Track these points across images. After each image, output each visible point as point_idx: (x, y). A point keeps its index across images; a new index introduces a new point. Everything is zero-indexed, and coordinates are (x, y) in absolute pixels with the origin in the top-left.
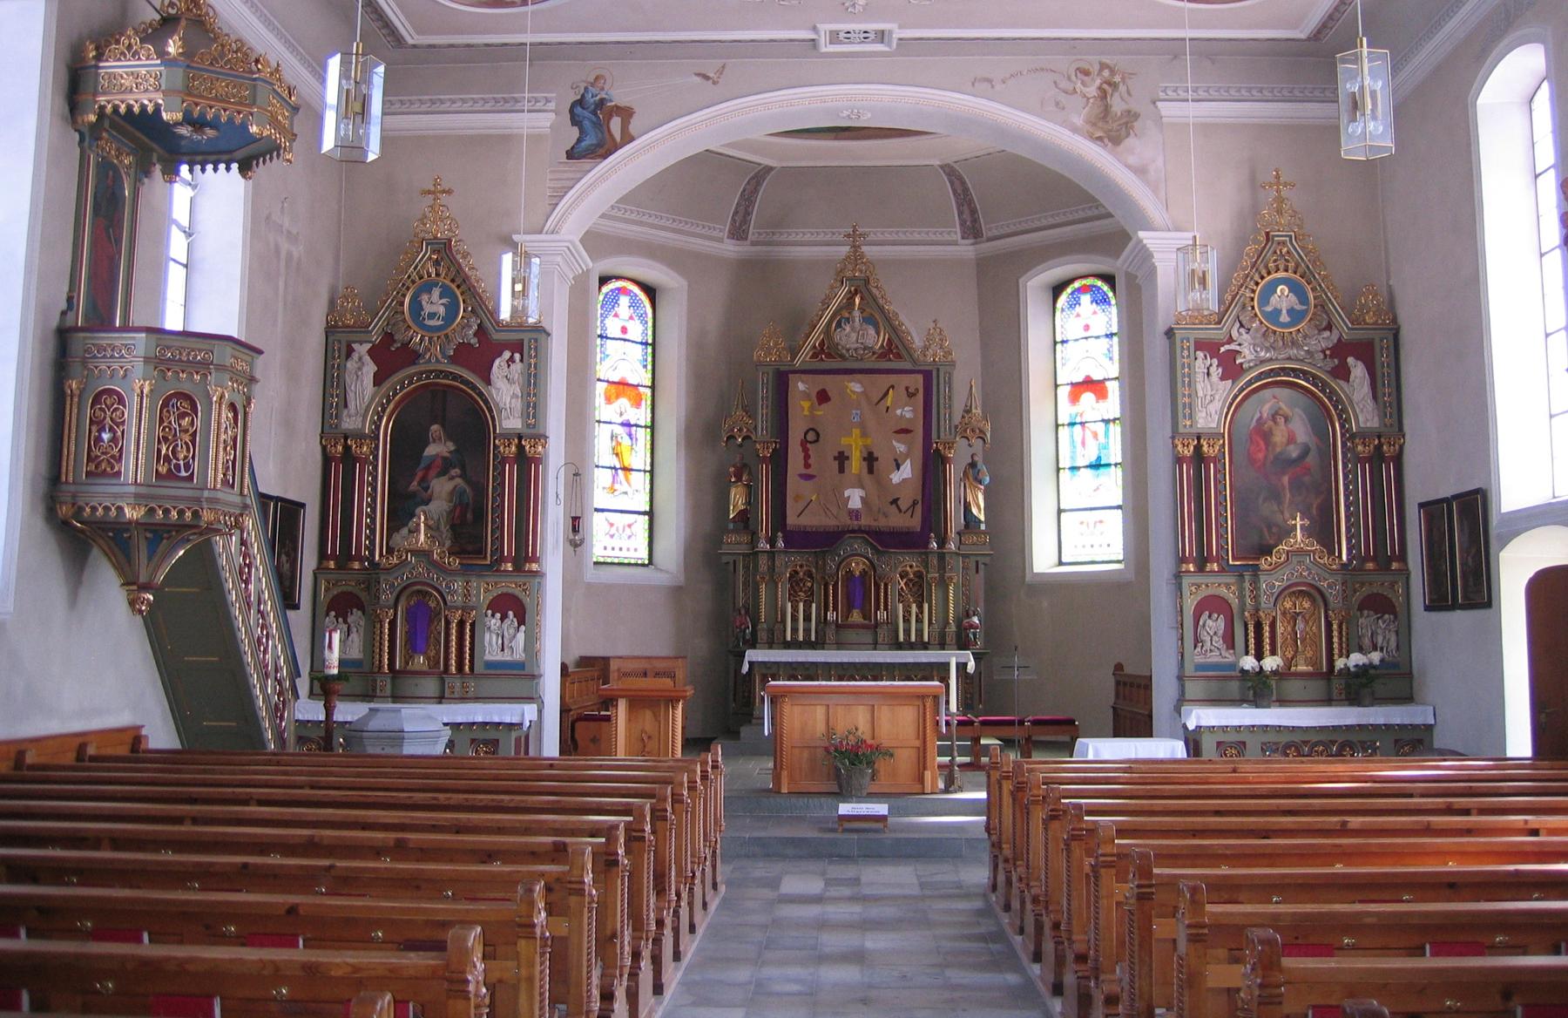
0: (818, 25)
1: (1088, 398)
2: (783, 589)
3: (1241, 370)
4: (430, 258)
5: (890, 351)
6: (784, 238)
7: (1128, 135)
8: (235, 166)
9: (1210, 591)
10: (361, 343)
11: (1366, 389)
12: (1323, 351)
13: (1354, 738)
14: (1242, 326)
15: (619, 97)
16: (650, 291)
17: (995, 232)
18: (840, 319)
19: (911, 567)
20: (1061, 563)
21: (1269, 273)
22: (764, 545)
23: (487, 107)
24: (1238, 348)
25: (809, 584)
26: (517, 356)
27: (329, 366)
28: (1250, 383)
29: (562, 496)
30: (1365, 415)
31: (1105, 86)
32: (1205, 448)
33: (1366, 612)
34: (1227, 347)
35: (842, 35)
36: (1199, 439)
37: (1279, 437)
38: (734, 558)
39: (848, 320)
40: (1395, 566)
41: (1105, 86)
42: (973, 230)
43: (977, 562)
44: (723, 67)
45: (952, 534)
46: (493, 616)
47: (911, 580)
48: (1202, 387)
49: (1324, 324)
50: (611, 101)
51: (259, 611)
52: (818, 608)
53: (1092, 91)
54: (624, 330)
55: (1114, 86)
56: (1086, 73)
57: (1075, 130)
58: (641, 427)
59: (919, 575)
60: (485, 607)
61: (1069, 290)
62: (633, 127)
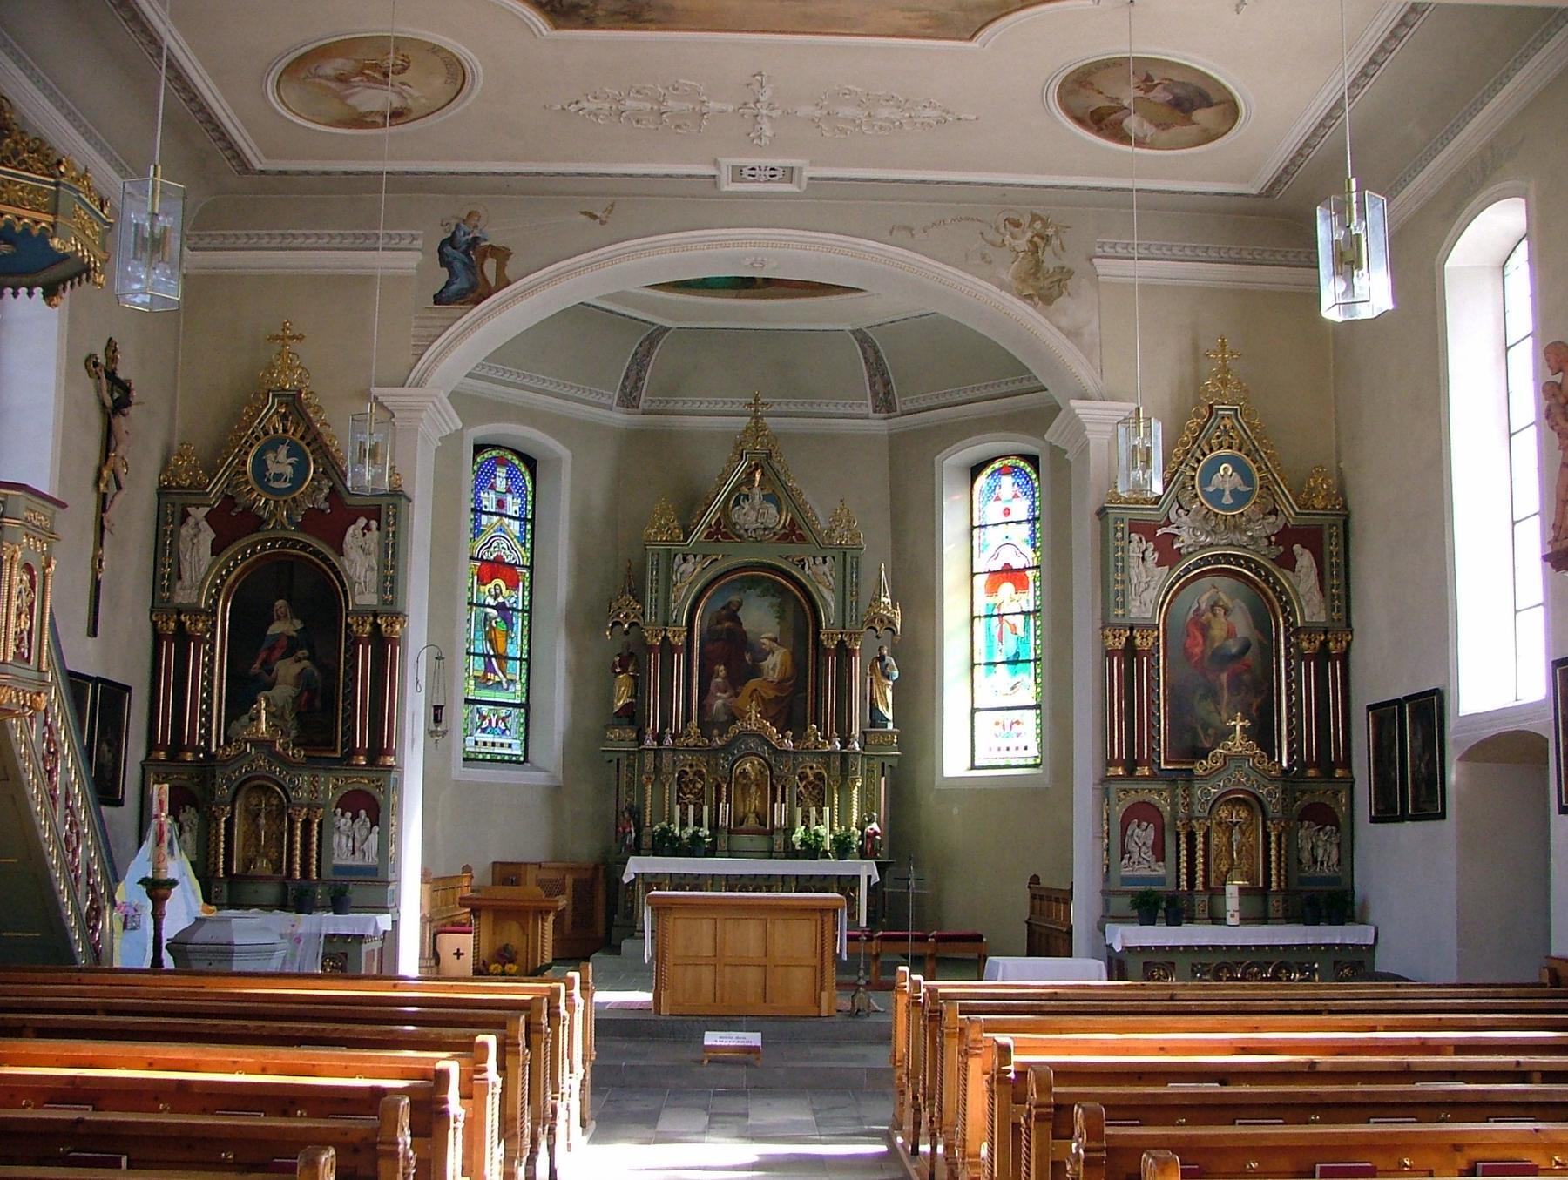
0: (719, 159)
1: (1007, 588)
2: (670, 791)
3: (1179, 556)
4: (276, 412)
5: (793, 532)
6: (679, 407)
7: (1061, 294)
8: (38, 291)
9: (1142, 797)
10: (197, 506)
11: (1313, 580)
12: (1268, 538)
13: (1291, 960)
14: (1181, 507)
15: (494, 236)
16: (530, 463)
17: (909, 406)
18: (738, 497)
19: (811, 768)
20: (973, 767)
21: (1211, 450)
22: (650, 742)
23: (346, 243)
24: (1176, 531)
25: (700, 786)
26: (374, 524)
27: (160, 532)
28: (1187, 570)
29: (423, 683)
30: (1312, 609)
31: (1036, 239)
32: (1138, 642)
33: (1306, 823)
34: (1165, 530)
35: (746, 172)
36: (1132, 629)
37: (1218, 631)
38: (620, 755)
39: (747, 497)
40: (1339, 773)
41: (1036, 239)
42: (885, 404)
43: (883, 764)
44: (612, 205)
45: (856, 732)
46: (343, 815)
47: (810, 783)
48: (1136, 573)
49: (1270, 507)
50: (486, 240)
51: (67, 807)
52: (710, 810)
53: (1022, 244)
54: (501, 504)
55: (1046, 239)
56: (1017, 225)
57: (1001, 286)
58: (518, 611)
59: (819, 776)
60: (334, 804)
61: (989, 470)
62: (509, 272)
